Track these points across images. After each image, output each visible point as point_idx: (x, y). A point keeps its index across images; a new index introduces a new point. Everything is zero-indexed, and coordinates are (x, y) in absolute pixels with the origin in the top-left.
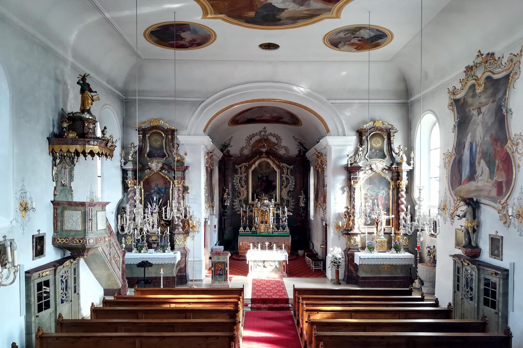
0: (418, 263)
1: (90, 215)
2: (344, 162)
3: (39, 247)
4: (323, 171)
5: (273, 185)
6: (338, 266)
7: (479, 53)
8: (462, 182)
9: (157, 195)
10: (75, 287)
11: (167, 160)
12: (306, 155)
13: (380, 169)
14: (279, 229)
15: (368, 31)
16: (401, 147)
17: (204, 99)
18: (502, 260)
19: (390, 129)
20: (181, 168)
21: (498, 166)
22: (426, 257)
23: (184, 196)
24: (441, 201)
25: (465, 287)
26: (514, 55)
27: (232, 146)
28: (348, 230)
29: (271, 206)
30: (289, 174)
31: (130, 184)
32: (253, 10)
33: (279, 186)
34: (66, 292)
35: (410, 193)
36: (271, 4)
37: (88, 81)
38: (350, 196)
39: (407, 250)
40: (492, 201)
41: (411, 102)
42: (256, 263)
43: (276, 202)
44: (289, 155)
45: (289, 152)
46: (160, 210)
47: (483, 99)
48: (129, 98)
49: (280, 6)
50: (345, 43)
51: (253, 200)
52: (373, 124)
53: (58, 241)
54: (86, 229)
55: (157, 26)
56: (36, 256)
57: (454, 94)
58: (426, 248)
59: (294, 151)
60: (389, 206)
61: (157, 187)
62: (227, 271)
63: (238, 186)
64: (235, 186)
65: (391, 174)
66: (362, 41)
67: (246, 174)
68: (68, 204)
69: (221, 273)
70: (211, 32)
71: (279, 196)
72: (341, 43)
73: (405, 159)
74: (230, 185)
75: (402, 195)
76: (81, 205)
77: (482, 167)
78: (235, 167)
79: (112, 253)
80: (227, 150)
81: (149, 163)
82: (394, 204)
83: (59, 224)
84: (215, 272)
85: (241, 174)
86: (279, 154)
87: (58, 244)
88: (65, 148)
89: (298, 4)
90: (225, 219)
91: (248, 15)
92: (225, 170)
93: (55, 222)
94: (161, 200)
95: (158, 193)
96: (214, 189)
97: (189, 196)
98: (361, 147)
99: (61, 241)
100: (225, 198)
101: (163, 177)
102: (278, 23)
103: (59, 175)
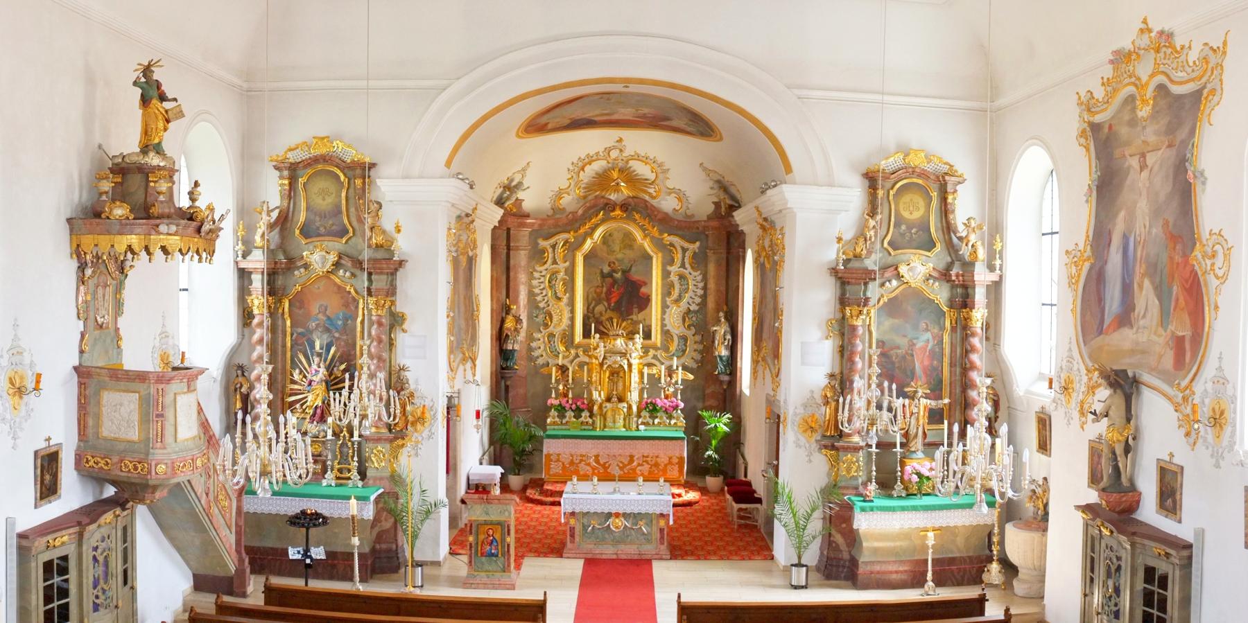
3: (47, 477)
5: (641, 295)
8: (1105, 327)
9: (325, 336)
10: (125, 572)
11: (349, 242)
12: (733, 216)
13: (920, 277)
17: (445, 82)
18: (1180, 521)
19: (946, 174)
21: (1177, 300)
23: (392, 340)
24: (1061, 367)
26: (1211, 48)
27: (528, 188)
30: (687, 265)
34: (106, 587)
37: (157, 75)
40: (1164, 381)
45: (690, 206)
46: (330, 375)
51: (586, 334)
52: (904, 159)
53: (88, 462)
56: (42, 498)
57: (1089, 110)
60: (940, 373)
61: (325, 314)
62: (509, 545)
67: (567, 264)
69: (493, 551)
71: (659, 323)
73: (982, 253)
75: (974, 346)
77: (1146, 298)
78: (538, 244)
79: (212, 489)
80: (514, 199)
85: (555, 262)
86: (659, 211)
93: (82, 416)
94: (333, 350)
95: (327, 330)
98: (872, 217)
101: (339, 287)
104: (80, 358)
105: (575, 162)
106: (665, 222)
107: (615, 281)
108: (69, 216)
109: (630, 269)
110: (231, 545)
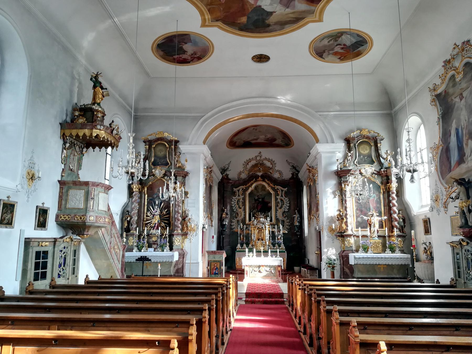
0: (415, 261)
1: (92, 194)
2: (335, 168)
4: (315, 181)
6: (333, 268)
7: (455, 46)
8: (452, 169)
13: (369, 173)
14: (275, 246)
15: (349, 36)
16: (389, 152)
17: (203, 114)
20: (181, 173)
22: (423, 256)
24: (433, 193)
25: (466, 269)
28: (341, 232)
29: (267, 224)
30: (283, 196)
31: (135, 188)
32: (244, 15)
33: (275, 207)
34: (64, 268)
35: (400, 197)
36: (260, 6)
37: (100, 79)
38: (342, 200)
39: (402, 252)
41: (395, 112)
42: (251, 269)
43: (272, 222)
44: (283, 178)
46: (161, 213)
47: (464, 85)
48: (138, 114)
49: (268, 9)
50: (329, 53)
51: (250, 220)
53: (61, 218)
54: (87, 207)
55: (162, 37)
58: (422, 244)
59: (287, 175)
62: (222, 270)
63: (235, 207)
64: (233, 207)
65: (381, 178)
66: (345, 49)
68: (73, 184)
69: (216, 272)
70: (209, 44)
71: (275, 217)
74: (228, 206)
75: (393, 197)
76: (85, 184)
79: (112, 242)
81: (153, 170)
82: (385, 207)
83: (63, 202)
86: (274, 178)
87: (60, 221)
88: (74, 132)
89: (284, 6)
90: (223, 238)
91: (241, 21)
92: (224, 192)
96: (213, 205)
97: (189, 201)
98: (349, 152)
99: (64, 217)
100: (224, 217)
102: (267, 29)
103: (68, 159)
104: (61, 178)
105: (245, 161)
106: (275, 182)
107: (260, 202)
109: (264, 198)
110: (119, 268)
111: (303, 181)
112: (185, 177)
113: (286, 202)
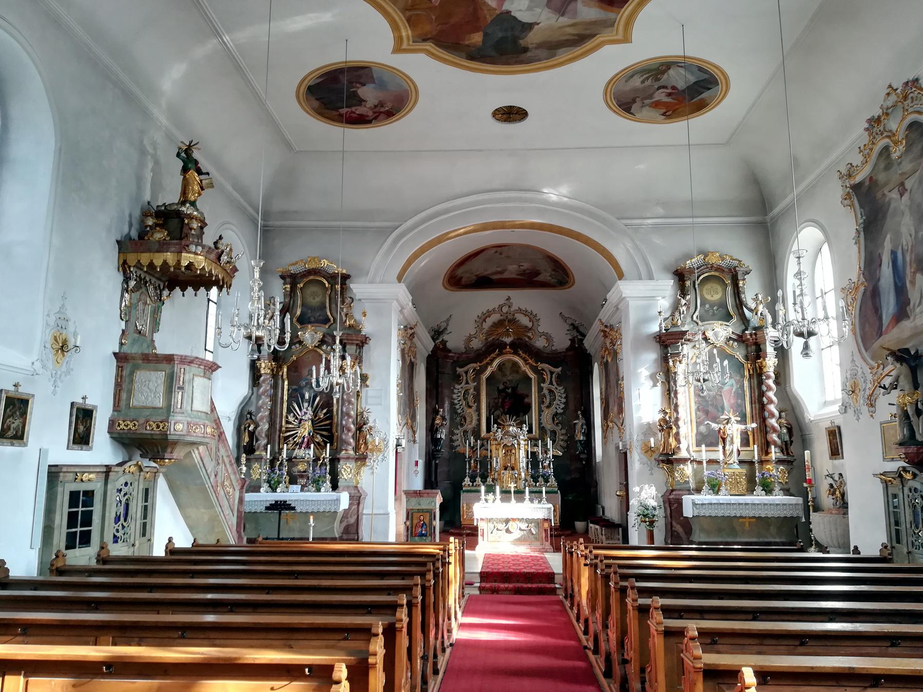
0: (811, 511)
1: (180, 380)
2: (654, 328)
4: (615, 354)
6: (652, 523)
7: (890, 89)
8: (883, 330)
13: (722, 339)
14: (538, 482)
15: (682, 71)
16: (760, 297)
17: (397, 224)
20: (355, 338)
22: (827, 501)
24: (846, 378)
25: (911, 527)
28: (667, 454)
29: (521, 437)
30: (554, 383)
31: (264, 368)
32: (477, 30)
33: (537, 404)
34: (125, 524)
35: (783, 385)
37: (196, 155)
38: (669, 390)
39: (787, 492)
41: (772, 219)
42: (491, 525)
43: (531, 435)
44: (554, 348)
46: (315, 416)
47: (907, 166)
48: (271, 223)
49: (524, 17)
50: (643, 103)
51: (489, 430)
53: (119, 425)
54: (171, 405)
55: (318, 72)
58: (826, 478)
59: (561, 342)
62: (434, 528)
63: (460, 406)
64: (456, 404)
65: (745, 348)
66: (674, 97)
68: (143, 360)
69: (423, 532)
70: (410, 87)
71: (537, 425)
72: (635, 102)
73: (769, 319)
74: (447, 402)
75: (769, 386)
76: (167, 360)
79: (220, 474)
81: (299, 333)
82: (753, 406)
83: (124, 396)
84: (412, 530)
86: (535, 348)
87: (117, 431)
88: (145, 258)
89: (556, 11)
90: (436, 465)
91: (471, 41)
92: (437, 376)
96: (417, 401)
97: (369, 392)
98: (683, 298)
99: (125, 425)
100: (437, 424)
102: (523, 57)
104: (120, 348)
105: (480, 315)
106: (537, 355)
107: (508, 394)
108: (119, 239)
109: (517, 386)
110: (232, 524)
111: (592, 354)
112: (363, 346)
113: (559, 394)
